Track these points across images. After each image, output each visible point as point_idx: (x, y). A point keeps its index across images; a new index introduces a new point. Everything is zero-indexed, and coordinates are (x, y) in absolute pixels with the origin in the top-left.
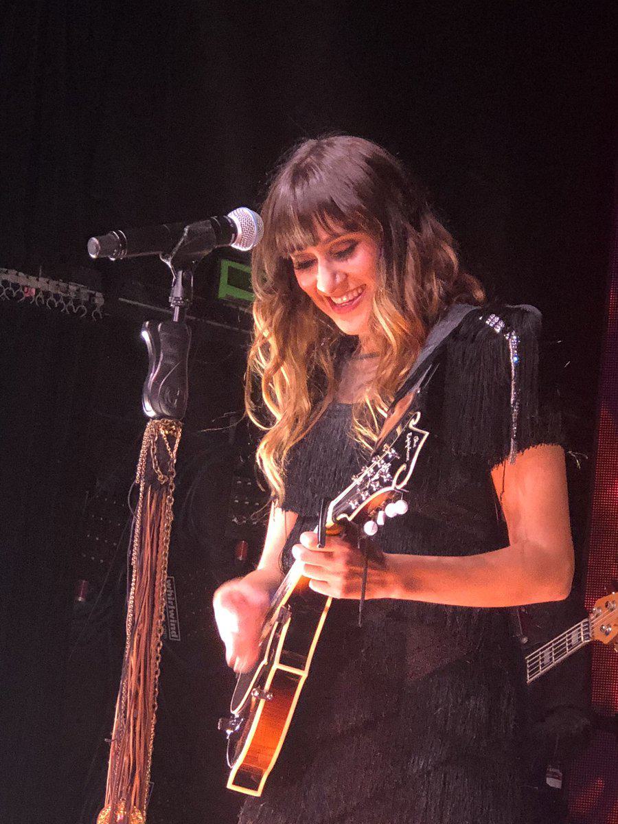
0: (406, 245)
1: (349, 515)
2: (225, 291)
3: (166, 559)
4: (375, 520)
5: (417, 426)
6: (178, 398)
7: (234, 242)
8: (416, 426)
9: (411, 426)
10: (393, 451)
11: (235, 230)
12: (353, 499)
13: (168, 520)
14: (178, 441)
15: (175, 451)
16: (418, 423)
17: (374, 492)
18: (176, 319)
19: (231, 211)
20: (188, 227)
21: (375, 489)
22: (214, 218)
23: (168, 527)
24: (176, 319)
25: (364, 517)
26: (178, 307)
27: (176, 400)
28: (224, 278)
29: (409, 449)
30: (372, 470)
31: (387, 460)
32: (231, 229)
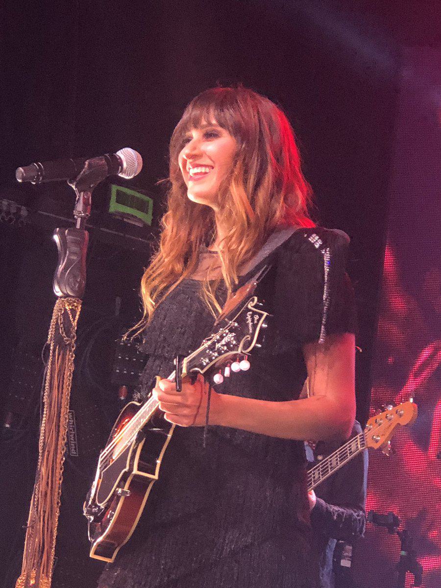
1: (202, 369)
8: (255, 307)
9: (249, 307)
11: (121, 164)
13: (71, 370)
14: (78, 313)
15: (76, 321)
18: (78, 226)
20: (87, 161)
21: (205, 364)
24: (78, 226)
26: (80, 218)
28: (114, 197)
32: (118, 163)
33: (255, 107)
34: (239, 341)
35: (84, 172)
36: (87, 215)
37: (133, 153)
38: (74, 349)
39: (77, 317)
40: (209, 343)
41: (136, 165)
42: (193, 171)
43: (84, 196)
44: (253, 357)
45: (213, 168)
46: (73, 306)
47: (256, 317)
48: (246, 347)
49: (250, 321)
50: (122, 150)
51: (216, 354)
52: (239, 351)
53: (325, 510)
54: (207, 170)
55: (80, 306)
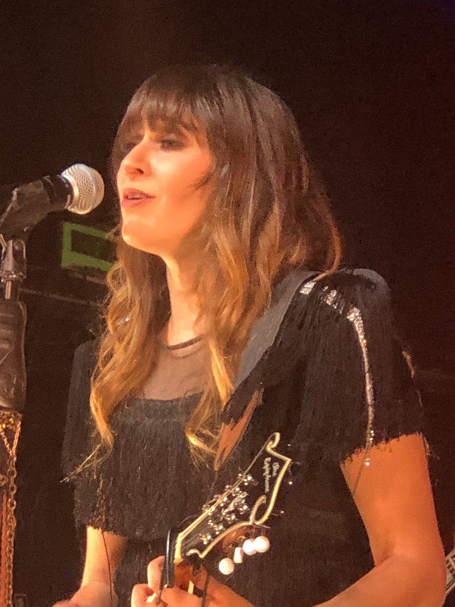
0: (271, 208)
1: (201, 551)
2: (70, 259)
3: (11, 572)
4: (232, 558)
5: (276, 449)
6: (14, 386)
7: (69, 205)
8: (276, 449)
9: (269, 449)
10: (250, 478)
11: (70, 190)
12: (205, 533)
13: (11, 527)
14: (17, 435)
15: (14, 447)
16: (279, 445)
17: (217, 536)
18: (8, 296)
19: (65, 168)
20: (16, 189)
21: (205, 543)
23: (10, 536)
24: (8, 296)
25: (219, 552)
26: (10, 283)
27: (13, 389)
28: (67, 241)
29: (268, 477)
30: (225, 499)
31: (242, 487)
32: (65, 190)
34: (251, 506)
35: (12, 208)
36: (21, 277)
38: (15, 492)
39: (16, 441)
40: (213, 508)
41: (95, 191)
43: (13, 247)
44: (272, 530)
46: (9, 423)
47: (276, 467)
50: (70, 169)
51: (221, 527)
52: (250, 523)
55: (20, 423)
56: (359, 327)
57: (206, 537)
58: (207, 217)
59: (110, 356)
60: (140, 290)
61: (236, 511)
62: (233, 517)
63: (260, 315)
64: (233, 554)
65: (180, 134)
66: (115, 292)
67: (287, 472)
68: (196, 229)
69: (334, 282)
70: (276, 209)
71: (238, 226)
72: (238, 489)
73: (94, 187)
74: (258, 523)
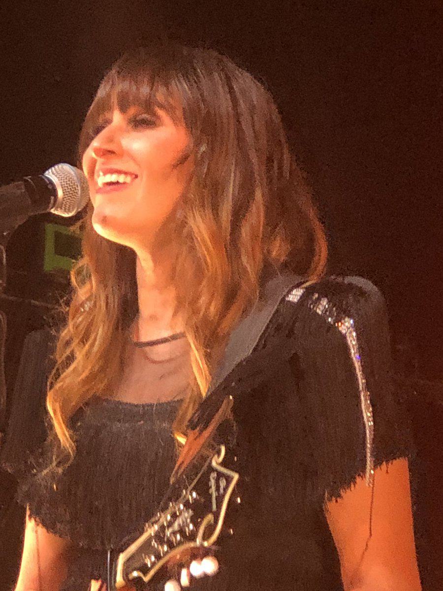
0: (252, 194)
4: (178, 580)
5: (224, 464)
7: (52, 208)
10: (194, 494)
11: (54, 192)
12: (148, 554)
19: (47, 169)
21: (149, 566)
22: (28, 178)
28: (50, 245)
29: (214, 495)
30: (169, 518)
31: (187, 505)
32: (49, 190)
33: (228, 81)
34: (197, 525)
37: (73, 173)
40: (156, 527)
41: (79, 192)
42: (102, 179)
44: (220, 552)
45: (136, 176)
48: (207, 536)
49: (213, 488)
50: (53, 168)
51: (166, 548)
53: (282, 165)
54: (128, 179)
56: (352, 341)
57: (150, 558)
58: (184, 200)
59: (71, 358)
60: (106, 286)
61: (181, 531)
62: (178, 537)
63: (245, 312)
64: (179, 574)
65: (154, 114)
66: (79, 290)
67: (234, 490)
68: (171, 217)
69: (325, 289)
70: (258, 194)
71: (216, 209)
72: (182, 507)
73: (79, 188)
74: (206, 544)
